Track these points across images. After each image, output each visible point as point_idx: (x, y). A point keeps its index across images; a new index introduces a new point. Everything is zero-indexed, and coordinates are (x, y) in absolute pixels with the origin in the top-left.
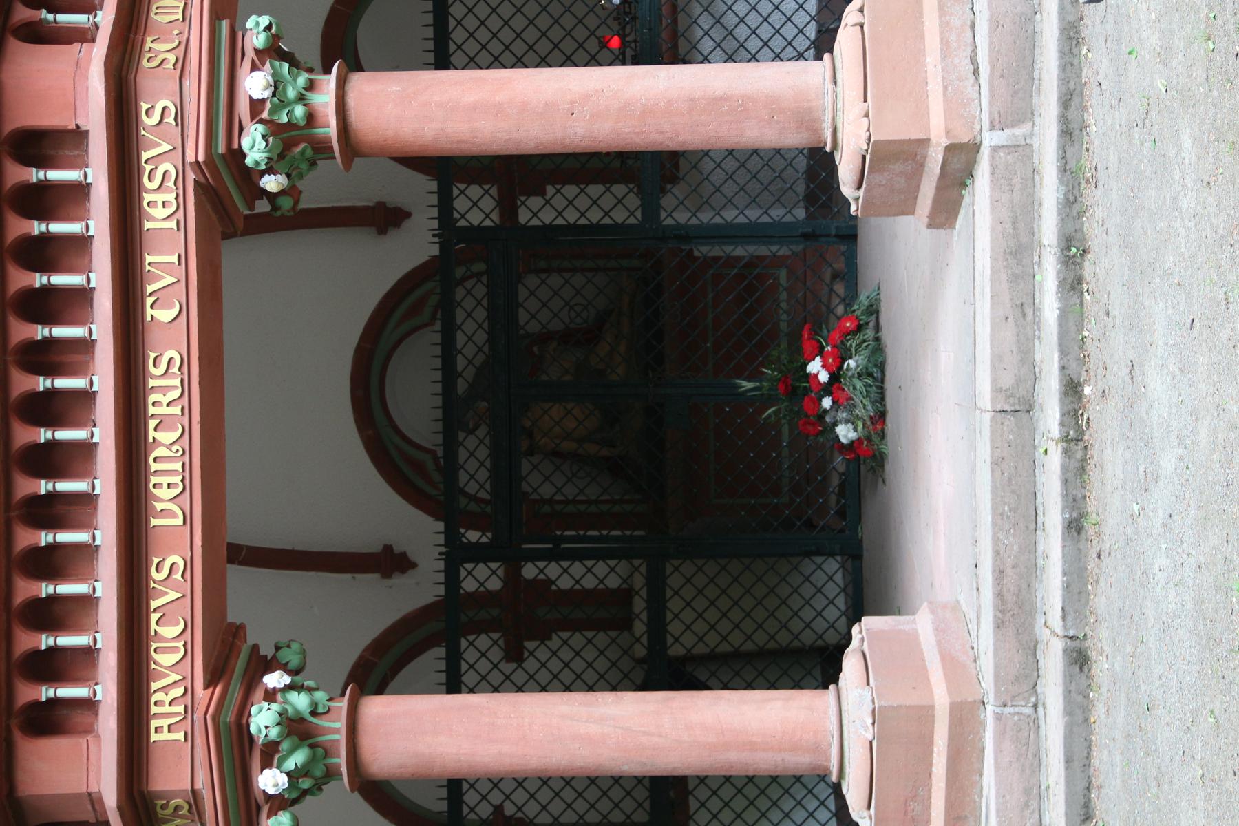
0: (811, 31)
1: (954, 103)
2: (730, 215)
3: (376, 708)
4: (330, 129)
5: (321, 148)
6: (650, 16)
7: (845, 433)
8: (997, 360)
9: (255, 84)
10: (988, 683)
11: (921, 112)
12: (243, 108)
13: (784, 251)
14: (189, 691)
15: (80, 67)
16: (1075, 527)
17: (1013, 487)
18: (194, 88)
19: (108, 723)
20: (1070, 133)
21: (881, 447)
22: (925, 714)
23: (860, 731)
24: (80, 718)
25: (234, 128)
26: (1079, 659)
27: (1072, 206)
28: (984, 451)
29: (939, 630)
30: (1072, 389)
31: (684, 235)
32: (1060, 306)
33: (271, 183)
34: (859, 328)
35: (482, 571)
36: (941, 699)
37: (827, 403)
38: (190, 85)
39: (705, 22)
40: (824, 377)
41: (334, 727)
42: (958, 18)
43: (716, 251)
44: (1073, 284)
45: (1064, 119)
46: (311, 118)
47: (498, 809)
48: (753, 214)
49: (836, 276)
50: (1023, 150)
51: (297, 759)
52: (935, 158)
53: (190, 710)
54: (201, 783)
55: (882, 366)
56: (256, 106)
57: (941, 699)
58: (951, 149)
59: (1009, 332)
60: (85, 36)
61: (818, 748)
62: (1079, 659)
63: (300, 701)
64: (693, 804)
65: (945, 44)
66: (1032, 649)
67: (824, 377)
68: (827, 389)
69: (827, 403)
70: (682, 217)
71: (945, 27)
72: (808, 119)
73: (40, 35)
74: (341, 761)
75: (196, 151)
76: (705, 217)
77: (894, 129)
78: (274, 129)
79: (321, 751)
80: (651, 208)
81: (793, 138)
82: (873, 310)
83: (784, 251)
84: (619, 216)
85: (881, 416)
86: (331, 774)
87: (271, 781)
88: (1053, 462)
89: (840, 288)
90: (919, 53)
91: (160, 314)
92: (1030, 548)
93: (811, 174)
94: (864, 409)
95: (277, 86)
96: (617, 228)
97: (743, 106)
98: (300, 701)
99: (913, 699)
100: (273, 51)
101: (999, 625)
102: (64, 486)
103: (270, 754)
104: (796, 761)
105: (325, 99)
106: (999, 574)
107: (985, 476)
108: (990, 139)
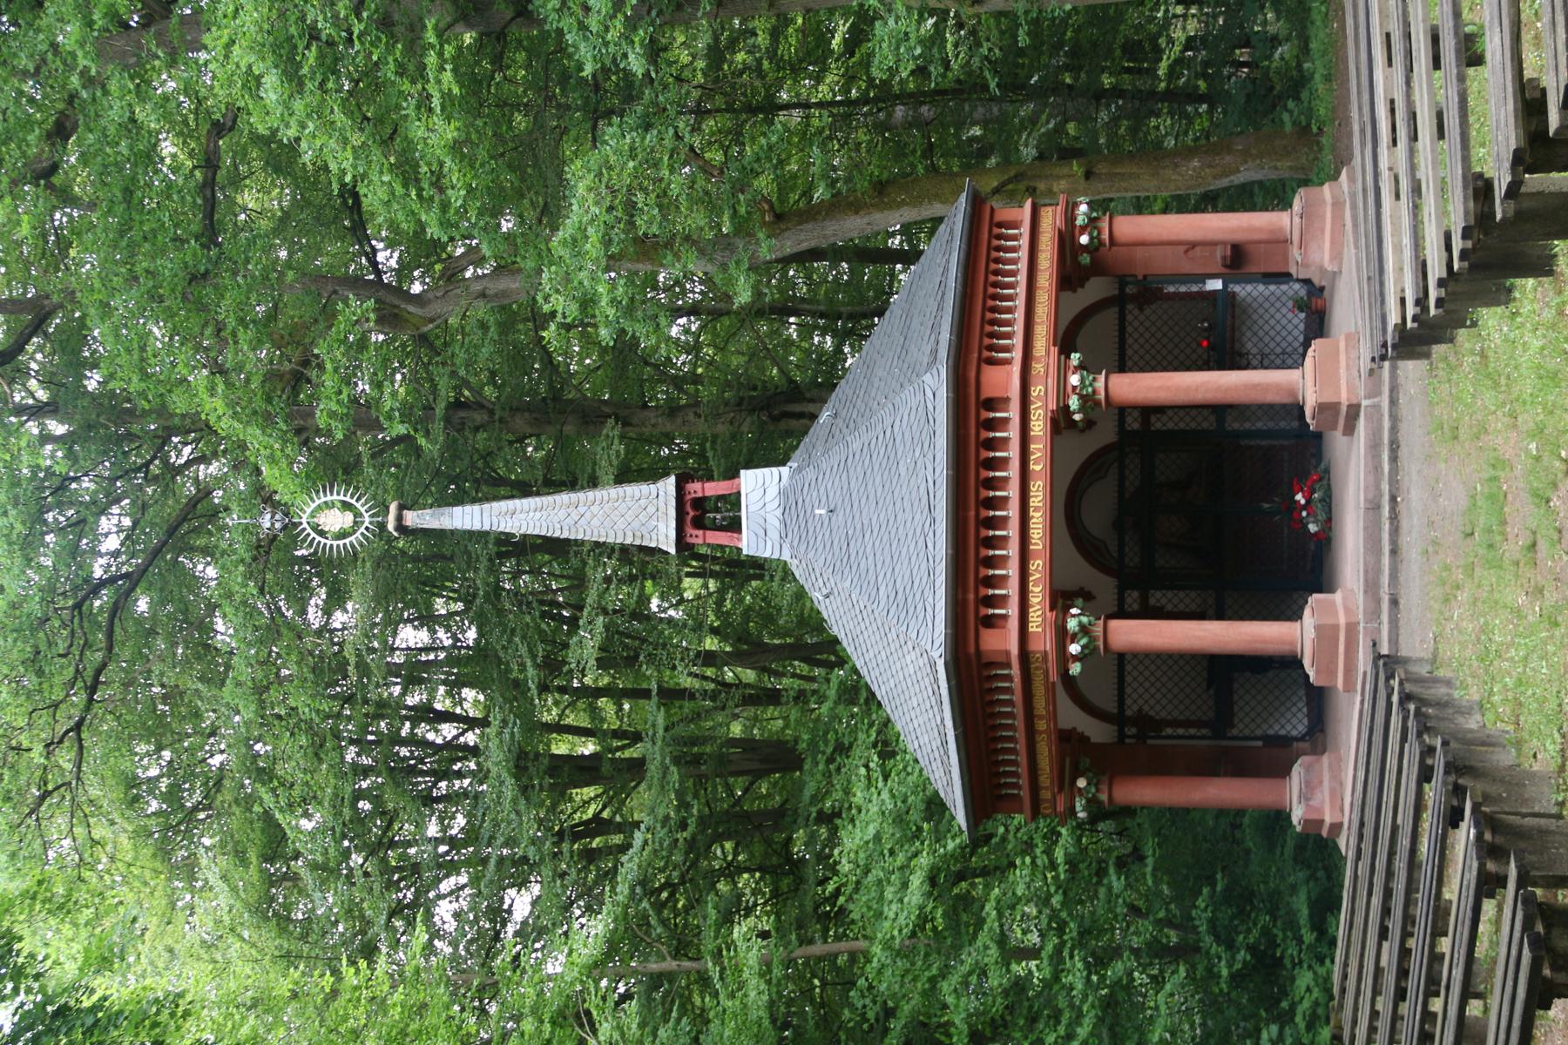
0: (1301, 338)
1: (1351, 388)
2: (1259, 425)
3: (1114, 624)
4: (1102, 396)
5: (1098, 403)
6: (1436, 958)
7: (1313, 528)
8: (1366, 488)
9: (1074, 380)
10: (1361, 616)
11: (1338, 393)
12: (1069, 389)
13: (1286, 443)
14: (1044, 613)
15: (1009, 374)
16: (1394, 552)
19: (1013, 624)
20: (1393, 402)
22: (1336, 627)
23: (1310, 634)
24: (1000, 622)
25: (1066, 397)
26: (1394, 602)
27: (1394, 429)
28: (1361, 524)
29: (1345, 599)
30: (1393, 499)
31: (1237, 435)
33: (1077, 417)
34: (1321, 479)
35: (1129, 600)
36: (1342, 620)
37: (1304, 514)
38: (1050, 381)
39: (1249, 334)
40: (1303, 502)
41: (1098, 629)
42: (1353, 355)
44: (1394, 459)
45: (1391, 397)
46: (1094, 392)
47: (1140, 710)
48: (1271, 425)
49: (1313, 455)
50: (1377, 407)
52: (1344, 409)
53: (1044, 620)
54: (1048, 647)
55: (1330, 497)
56: (1074, 388)
57: (1342, 620)
58: (1349, 406)
59: (1371, 478)
60: (1008, 362)
61: (1293, 643)
62: (1394, 602)
63: (1085, 620)
64: (1236, 709)
65: (1348, 365)
66: (1378, 601)
67: (1303, 502)
68: (1304, 507)
69: (1304, 514)
70: (1236, 426)
71: (1348, 358)
72: (1292, 392)
73: (992, 362)
74: (1101, 643)
75: (1052, 406)
76: (1247, 425)
77: (1328, 398)
78: (1081, 397)
79: (1093, 639)
81: (1287, 400)
82: (1327, 471)
83: (1286, 443)
84: (1205, 425)
85: (1329, 520)
86: (1096, 648)
87: (1074, 649)
88: (1386, 527)
89: (1313, 461)
90: (1338, 369)
91: (1036, 467)
92: (1379, 562)
93: (1296, 412)
94: (1322, 516)
95: (1082, 380)
98: (1085, 620)
99: (1331, 621)
100: (1081, 367)
101: (1366, 592)
102: (998, 533)
103: (1074, 639)
104: (1284, 649)
105: (1100, 384)
106: (1366, 572)
108: (1364, 403)
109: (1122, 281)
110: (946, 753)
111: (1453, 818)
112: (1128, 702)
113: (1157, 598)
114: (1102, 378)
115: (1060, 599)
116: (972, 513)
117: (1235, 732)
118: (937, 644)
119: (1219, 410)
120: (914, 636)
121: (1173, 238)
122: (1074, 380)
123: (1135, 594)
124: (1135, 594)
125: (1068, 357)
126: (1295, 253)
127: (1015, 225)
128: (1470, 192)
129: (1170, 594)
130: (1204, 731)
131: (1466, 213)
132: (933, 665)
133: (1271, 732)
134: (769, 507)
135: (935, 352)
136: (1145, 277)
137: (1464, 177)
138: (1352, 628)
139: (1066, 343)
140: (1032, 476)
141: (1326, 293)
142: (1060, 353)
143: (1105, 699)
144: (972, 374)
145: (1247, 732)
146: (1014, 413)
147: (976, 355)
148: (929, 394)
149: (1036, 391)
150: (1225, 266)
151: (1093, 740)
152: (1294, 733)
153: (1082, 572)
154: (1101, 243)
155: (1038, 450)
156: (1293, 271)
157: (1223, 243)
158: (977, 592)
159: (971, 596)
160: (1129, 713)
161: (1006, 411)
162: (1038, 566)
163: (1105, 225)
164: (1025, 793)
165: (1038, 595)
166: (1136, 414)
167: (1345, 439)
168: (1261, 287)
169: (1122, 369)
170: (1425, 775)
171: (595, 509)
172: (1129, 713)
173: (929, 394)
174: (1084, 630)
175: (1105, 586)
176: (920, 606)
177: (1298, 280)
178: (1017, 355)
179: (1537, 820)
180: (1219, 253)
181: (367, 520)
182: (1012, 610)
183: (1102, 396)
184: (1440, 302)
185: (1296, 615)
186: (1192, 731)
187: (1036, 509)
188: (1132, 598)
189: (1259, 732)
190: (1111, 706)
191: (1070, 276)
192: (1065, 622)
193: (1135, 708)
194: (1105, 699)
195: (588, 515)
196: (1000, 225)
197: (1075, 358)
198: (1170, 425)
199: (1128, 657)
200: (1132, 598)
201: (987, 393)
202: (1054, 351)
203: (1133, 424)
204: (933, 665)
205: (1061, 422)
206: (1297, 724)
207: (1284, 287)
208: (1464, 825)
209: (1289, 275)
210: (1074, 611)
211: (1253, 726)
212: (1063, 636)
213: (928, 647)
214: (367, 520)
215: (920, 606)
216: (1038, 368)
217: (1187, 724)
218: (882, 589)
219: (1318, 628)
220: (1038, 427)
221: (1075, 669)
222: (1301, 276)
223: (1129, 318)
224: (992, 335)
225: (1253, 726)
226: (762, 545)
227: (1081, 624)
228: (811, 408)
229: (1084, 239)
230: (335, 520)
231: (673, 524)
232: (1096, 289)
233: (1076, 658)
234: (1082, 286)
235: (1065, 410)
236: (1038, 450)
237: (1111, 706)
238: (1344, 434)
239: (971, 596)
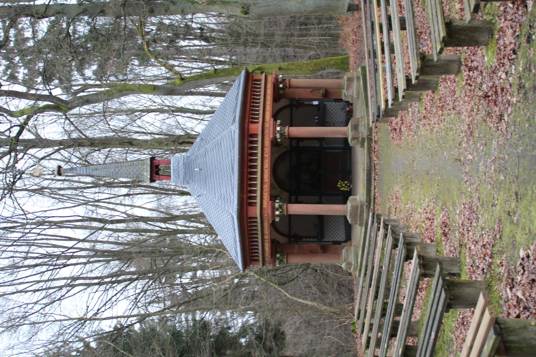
3: (290, 205)
4: (287, 134)
8: (367, 164)
9: (278, 129)
14: (268, 202)
17: (490, 260)
18: (271, 129)
21: (8, 63)
25: (276, 134)
32: (455, 24)
33: (279, 140)
43: (331, 151)
51: (280, 210)
60: (257, 123)
70: (326, 146)
74: (285, 211)
75: (271, 136)
76: (329, 146)
80: (321, 144)
84: (317, 145)
87: (277, 213)
95: (281, 129)
96: (317, 147)
97: (336, 132)
98: (280, 204)
103: (277, 210)
107: (365, 175)
109: (292, 100)
110: (236, 246)
111: (408, 257)
112: (292, 230)
113: (300, 198)
114: (287, 128)
115: (273, 198)
116: (246, 170)
117: (324, 240)
118: (234, 211)
119: (320, 140)
120: (227, 209)
121: (306, 86)
122: (278, 129)
123: (294, 197)
124: (294, 197)
125: (276, 122)
126: (344, 91)
127: (260, 80)
128: (419, 58)
129: (305, 197)
130: (315, 240)
131: (418, 65)
132: (233, 218)
133: (335, 240)
134: (180, 168)
135: (235, 118)
136: (299, 99)
137: (417, 54)
138: (362, 206)
139: (275, 116)
141: (354, 105)
142: (274, 120)
143: (285, 230)
144: (246, 126)
145: (328, 240)
146: (259, 139)
148: (233, 132)
149: (267, 131)
150: (323, 96)
151: (281, 242)
152: (342, 240)
153: (278, 190)
154: (286, 87)
156: (343, 98)
157: (323, 88)
158: (247, 194)
159: (245, 196)
160: (292, 234)
161: (257, 138)
162: (266, 187)
164: (260, 259)
165: (266, 196)
166: (295, 141)
167: (361, 149)
168: (334, 103)
169: (291, 126)
170: (395, 246)
171: (124, 168)
172: (292, 234)
173: (233, 132)
174: (280, 207)
175: (286, 195)
176: (229, 199)
177: (345, 101)
178: (261, 120)
180: (321, 91)
182: (258, 201)
183: (287, 134)
184: (392, 105)
185: (345, 202)
186: (311, 240)
187: (266, 169)
188: (293, 197)
189: (331, 240)
190: (286, 231)
191: (276, 98)
192: (274, 204)
193: (294, 232)
194: (285, 230)
195: (121, 170)
196: (255, 80)
197: (279, 122)
198: (306, 145)
199: (292, 216)
200: (293, 197)
201: (251, 132)
202: (272, 119)
203: (294, 143)
204: (233, 218)
205: (274, 143)
206: (341, 237)
207: (341, 103)
208: (413, 261)
209: (342, 100)
210: (277, 201)
211: (330, 238)
212: (274, 209)
213: (231, 212)
215: (229, 199)
216: (267, 125)
217: (310, 237)
218: (217, 194)
219: (352, 207)
220: (267, 143)
221: (277, 220)
222: (346, 100)
223: (294, 111)
224: (253, 114)
225: (330, 238)
227: (280, 206)
228: (192, 140)
229: (281, 86)
231: (149, 173)
232: (283, 102)
233: (278, 216)
234: (279, 101)
235: (275, 138)
237: (286, 231)
238: (361, 147)
239: (245, 196)
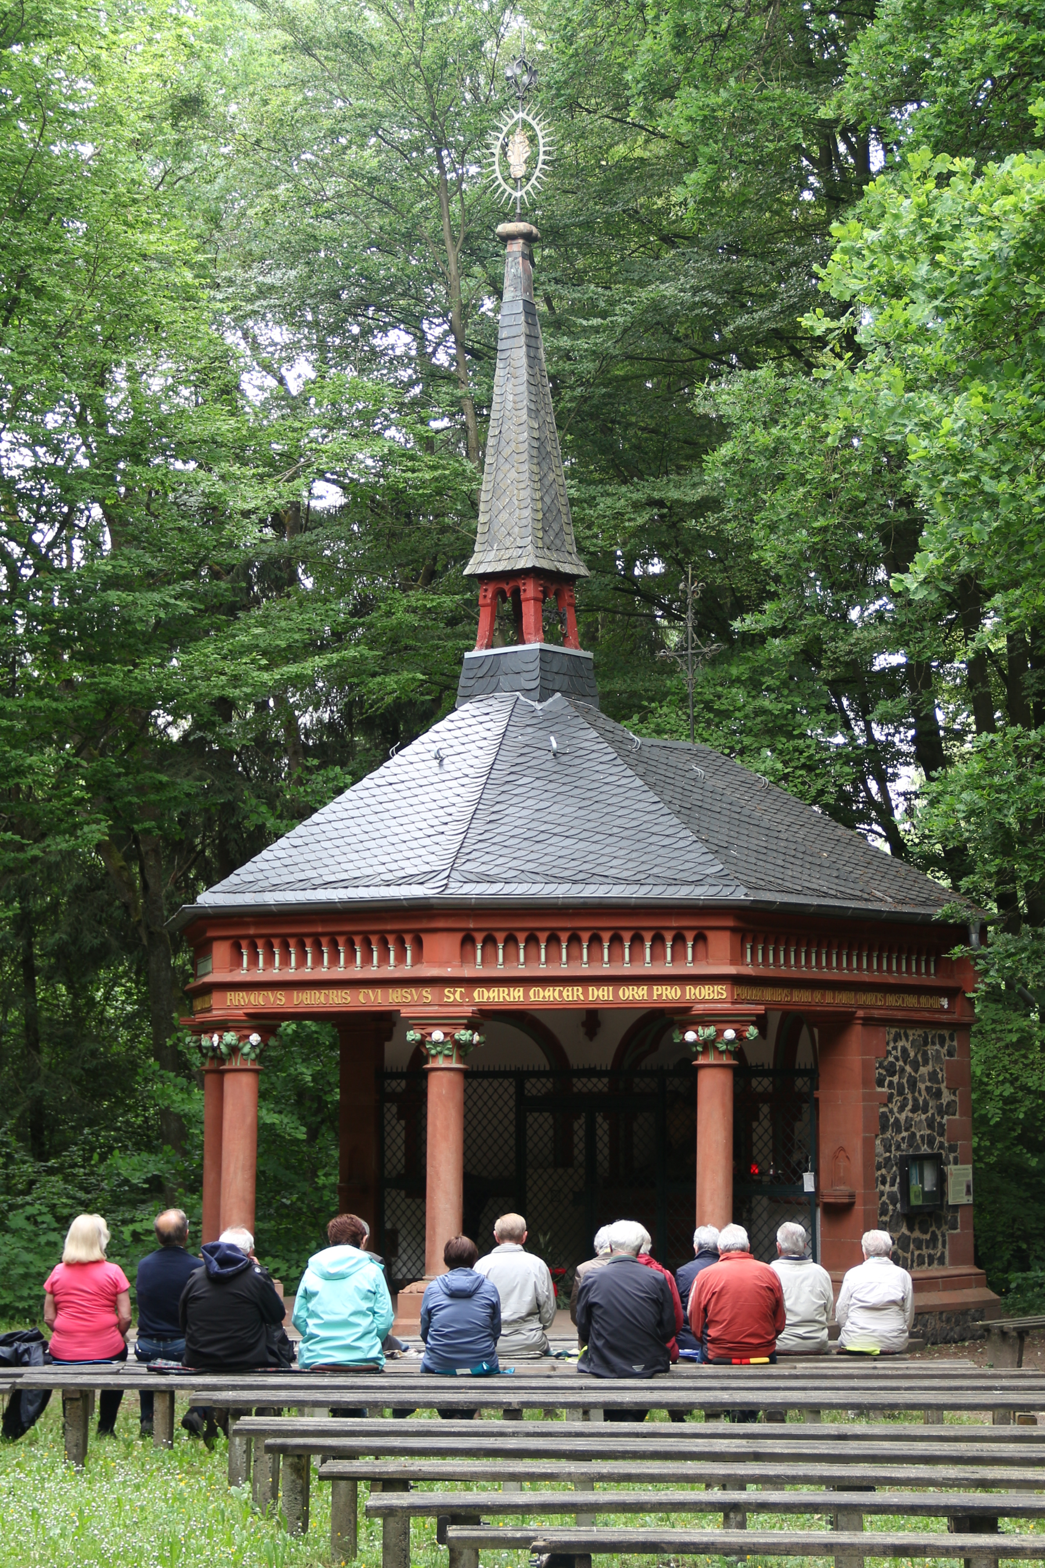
9: (438, 1035)
15: (447, 963)
74: (226, 1067)
75: (405, 1012)
78: (421, 1043)
140: (354, 992)
142: (758, 1016)
147: (320, 929)
149: (427, 994)
155: (572, 995)
163: (711, 1059)
179: (978, 1445)
181: (518, 194)
214: (518, 194)
220: (669, 994)
226: (471, 674)
230: (518, 153)
236: (572, 995)
